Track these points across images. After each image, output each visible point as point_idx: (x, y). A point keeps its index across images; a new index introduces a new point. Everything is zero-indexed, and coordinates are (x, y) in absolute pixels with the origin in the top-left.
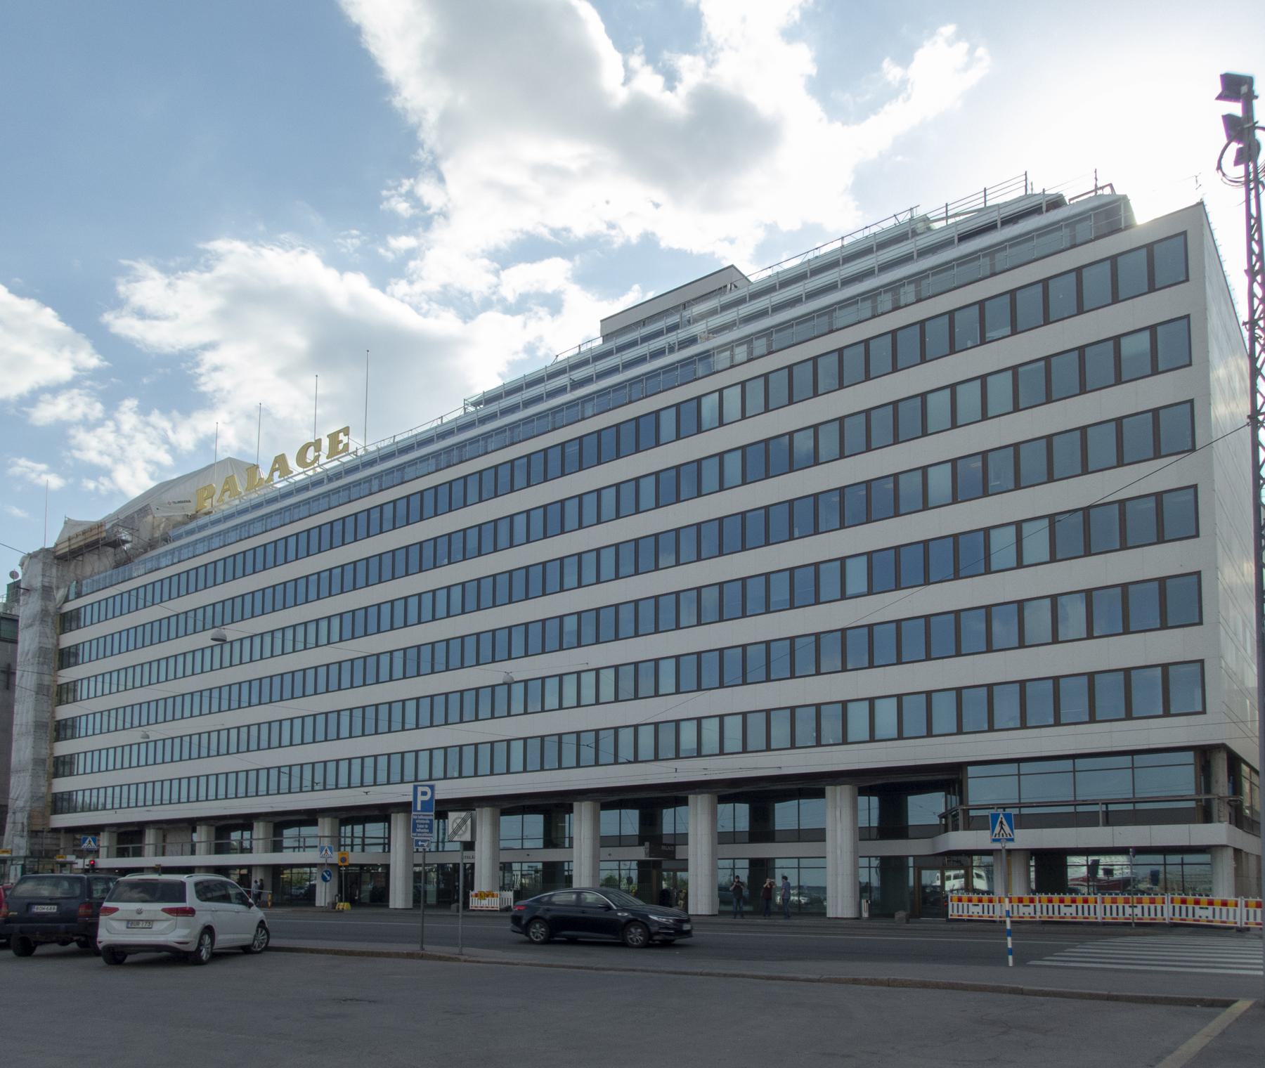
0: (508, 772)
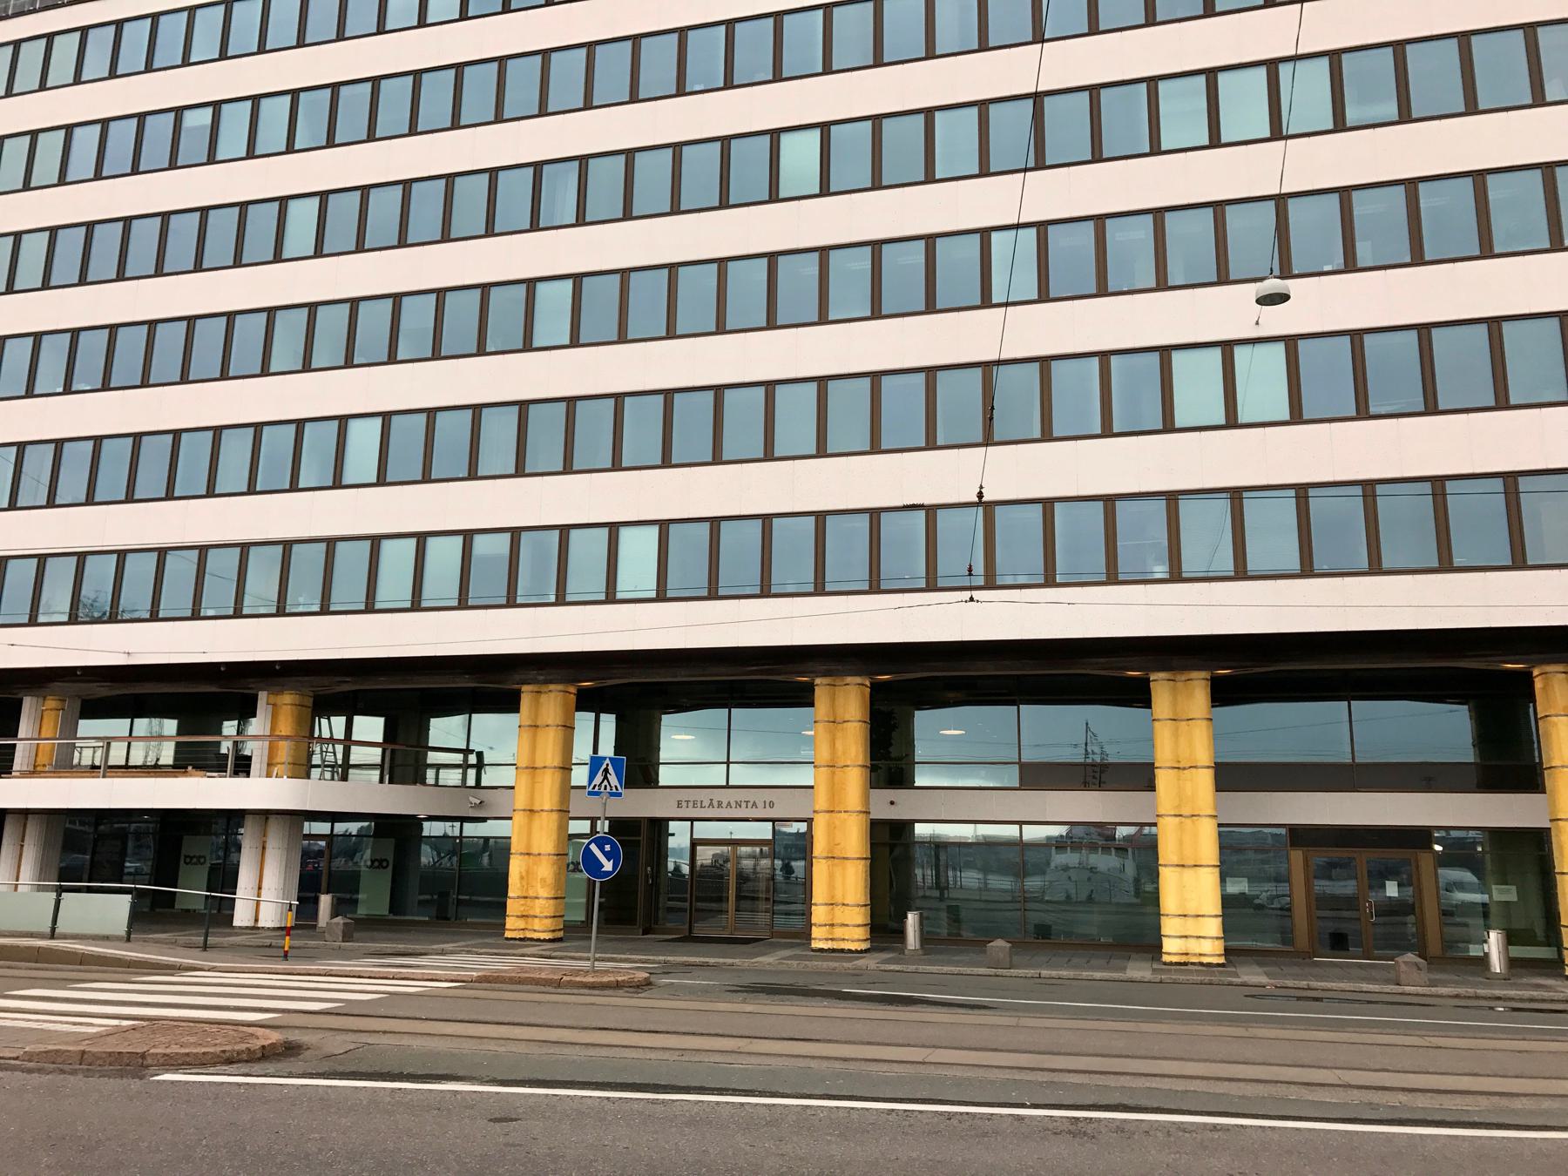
0: (611, 597)
